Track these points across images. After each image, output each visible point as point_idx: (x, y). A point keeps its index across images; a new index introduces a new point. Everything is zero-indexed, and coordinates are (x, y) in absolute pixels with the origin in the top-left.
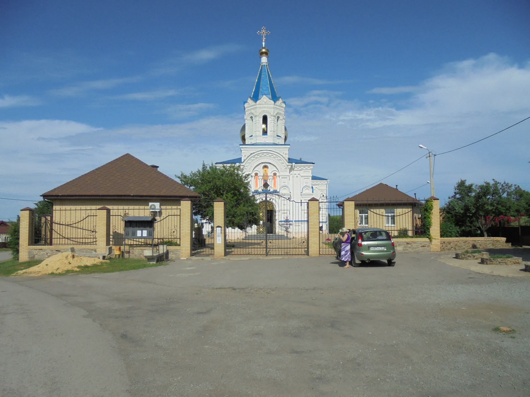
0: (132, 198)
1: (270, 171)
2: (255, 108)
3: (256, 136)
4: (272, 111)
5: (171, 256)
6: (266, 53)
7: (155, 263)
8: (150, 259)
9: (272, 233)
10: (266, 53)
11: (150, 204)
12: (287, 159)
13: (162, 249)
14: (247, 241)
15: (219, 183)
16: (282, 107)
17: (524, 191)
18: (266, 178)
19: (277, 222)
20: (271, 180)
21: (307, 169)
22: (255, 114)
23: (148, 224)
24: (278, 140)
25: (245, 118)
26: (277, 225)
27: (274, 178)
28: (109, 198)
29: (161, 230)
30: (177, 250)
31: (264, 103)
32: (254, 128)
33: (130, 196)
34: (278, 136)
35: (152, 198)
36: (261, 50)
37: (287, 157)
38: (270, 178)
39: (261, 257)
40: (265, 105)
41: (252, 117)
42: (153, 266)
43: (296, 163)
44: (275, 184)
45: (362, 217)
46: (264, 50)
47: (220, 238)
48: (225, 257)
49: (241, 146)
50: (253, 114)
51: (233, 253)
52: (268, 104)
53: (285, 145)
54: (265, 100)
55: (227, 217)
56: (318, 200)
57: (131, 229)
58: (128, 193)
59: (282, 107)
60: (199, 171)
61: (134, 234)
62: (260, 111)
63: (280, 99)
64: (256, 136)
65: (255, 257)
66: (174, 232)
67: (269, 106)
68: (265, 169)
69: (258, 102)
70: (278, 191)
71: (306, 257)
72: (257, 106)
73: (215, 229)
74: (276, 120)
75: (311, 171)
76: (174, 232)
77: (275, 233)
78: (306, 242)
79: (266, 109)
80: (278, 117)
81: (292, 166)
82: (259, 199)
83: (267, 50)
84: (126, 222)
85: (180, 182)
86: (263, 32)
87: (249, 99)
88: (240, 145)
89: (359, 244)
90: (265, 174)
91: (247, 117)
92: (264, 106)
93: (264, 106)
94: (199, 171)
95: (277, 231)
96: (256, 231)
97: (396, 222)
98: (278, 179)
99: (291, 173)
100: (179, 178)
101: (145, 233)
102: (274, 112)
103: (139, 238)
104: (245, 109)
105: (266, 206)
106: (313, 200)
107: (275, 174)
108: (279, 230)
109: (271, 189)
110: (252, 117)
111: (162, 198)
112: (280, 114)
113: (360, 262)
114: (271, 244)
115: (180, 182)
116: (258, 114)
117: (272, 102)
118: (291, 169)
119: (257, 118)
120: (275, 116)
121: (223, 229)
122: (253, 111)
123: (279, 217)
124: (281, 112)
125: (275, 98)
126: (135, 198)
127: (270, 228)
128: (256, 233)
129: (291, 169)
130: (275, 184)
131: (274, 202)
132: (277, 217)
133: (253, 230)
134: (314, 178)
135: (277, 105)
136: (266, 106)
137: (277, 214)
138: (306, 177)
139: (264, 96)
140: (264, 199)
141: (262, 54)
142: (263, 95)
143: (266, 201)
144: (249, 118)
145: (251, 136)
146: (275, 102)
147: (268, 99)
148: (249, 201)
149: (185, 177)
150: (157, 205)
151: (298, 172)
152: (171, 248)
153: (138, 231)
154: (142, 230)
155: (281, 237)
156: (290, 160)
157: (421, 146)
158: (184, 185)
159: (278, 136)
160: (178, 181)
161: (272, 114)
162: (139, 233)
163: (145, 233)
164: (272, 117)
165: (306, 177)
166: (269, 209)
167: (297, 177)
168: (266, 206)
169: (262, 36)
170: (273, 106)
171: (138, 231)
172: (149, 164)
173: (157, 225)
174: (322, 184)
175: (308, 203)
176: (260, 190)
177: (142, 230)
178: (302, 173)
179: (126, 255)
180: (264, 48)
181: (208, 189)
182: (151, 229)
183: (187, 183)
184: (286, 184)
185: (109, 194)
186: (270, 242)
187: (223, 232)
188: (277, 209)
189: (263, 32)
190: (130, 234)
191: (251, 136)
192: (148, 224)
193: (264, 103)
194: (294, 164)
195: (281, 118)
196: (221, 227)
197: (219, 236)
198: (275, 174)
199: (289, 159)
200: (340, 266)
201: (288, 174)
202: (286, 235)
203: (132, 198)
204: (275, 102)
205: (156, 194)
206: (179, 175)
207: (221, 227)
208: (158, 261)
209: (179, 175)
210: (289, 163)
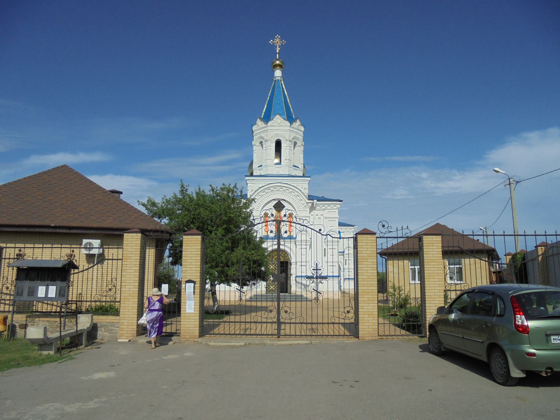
0: (54, 231)
3: (266, 166)
5: (101, 334)
6: (280, 66)
7: (52, 353)
8: (44, 344)
9: (287, 292)
10: (280, 66)
11: (85, 241)
12: (307, 195)
13: (84, 322)
14: (254, 304)
15: (205, 214)
16: (301, 131)
19: (293, 278)
21: (332, 209)
22: (266, 138)
23: (61, 274)
24: (295, 171)
25: (253, 143)
28: (11, 229)
29: (86, 285)
30: (113, 324)
31: (277, 125)
32: (262, 156)
33: (49, 227)
34: (294, 166)
35: (88, 232)
36: (274, 62)
37: (306, 192)
39: (268, 341)
40: (279, 127)
41: (261, 143)
42: (49, 360)
43: (318, 201)
45: (414, 271)
46: (278, 62)
47: (192, 303)
48: (200, 340)
49: (246, 178)
50: (263, 138)
51: (216, 331)
53: (303, 176)
54: (279, 122)
55: (206, 263)
56: (375, 234)
57: (27, 284)
58: (46, 222)
59: (301, 131)
60: (175, 197)
61: (33, 292)
63: (298, 121)
65: (256, 340)
66: (110, 290)
69: (270, 123)
71: (353, 340)
72: (269, 128)
73: (183, 286)
74: (293, 146)
75: (337, 211)
76: (110, 290)
77: (290, 293)
78: (352, 311)
79: (280, 132)
80: (295, 144)
81: (313, 204)
82: (269, 246)
83: (282, 62)
84: (19, 269)
85: (146, 212)
86: (277, 41)
87: (259, 120)
88: (246, 176)
89: (517, 327)
91: (256, 142)
92: (278, 128)
93: (278, 128)
94: (175, 197)
95: (293, 289)
96: (265, 289)
97: (464, 277)
99: (312, 213)
100: (143, 205)
101: (53, 291)
102: (290, 136)
103: (42, 300)
104: (253, 132)
105: (279, 256)
106: (366, 232)
108: (294, 288)
110: (261, 143)
111: (108, 232)
112: (298, 139)
113: (523, 375)
114: (287, 315)
115: (146, 212)
116: (269, 138)
117: (288, 123)
118: (312, 208)
119: (268, 143)
120: (291, 141)
121: (198, 285)
122: (262, 135)
124: (298, 136)
125: (290, 119)
126: (58, 231)
127: (284, 287)
128: (264, 293)
129: (312, 208)
131: (287, 250)
133: (261, 287)
134: (340, 224)
135: (293, 128)
136: (280, 128)
137: (293, 266)
138: (331, 219)
139: (278, 116)
140: (276, 247)
141: (275, 66)
142: (275, 115)
143: (279, 250)
144: (258, 144)
145: (261, 166)
146: (291, 123)
147: (282, 120)
148: (250, 241)
149: (154, 204)
150: (96, 243)
152: (100, 319)
153: (40, 288)
154: (47, 286)
155: (300, 298)
156: (310, 198)
157: (496, 169)
158: (153, 217)
159: (294, 166)
160: (143, 209)
161: (287, 138)
162: (41, 291)
163: (53, 291)
164: (288, 142)
165: (331, 219)
166: (282, 260)
167: (319, 218)
168: (279, 256)
169: (276, 46)
170: (289, 128)
171: (40, 288)
172: (108, 188)
173: (74, 278)
175: (355, 239)
177: (47, 286)
178: (326, 214)
179: (20, 332)
180: (278, 60)
181: (185, 221)
182: (64, 284)
183: (155, 214)
185: (13, 223)
186: (286, 312)
187: (198, 291)
188: (293, 260)
189: (277, 41)
190: (26, 292)
191: (261, 166)
192: (61, 274)
193: (277, 125)
194: (315, 201)
195: (299, 143)
196: (194, 282)
197: (190, 299)
199: (309, 196)
202: (305, 296)
203: (54, 231)
204: (291, 123)
205: (95, 225)
206: (145, 201)
207: (194, 282)
208: (59, 350)
209: (145, 201)
210: (309, 199)
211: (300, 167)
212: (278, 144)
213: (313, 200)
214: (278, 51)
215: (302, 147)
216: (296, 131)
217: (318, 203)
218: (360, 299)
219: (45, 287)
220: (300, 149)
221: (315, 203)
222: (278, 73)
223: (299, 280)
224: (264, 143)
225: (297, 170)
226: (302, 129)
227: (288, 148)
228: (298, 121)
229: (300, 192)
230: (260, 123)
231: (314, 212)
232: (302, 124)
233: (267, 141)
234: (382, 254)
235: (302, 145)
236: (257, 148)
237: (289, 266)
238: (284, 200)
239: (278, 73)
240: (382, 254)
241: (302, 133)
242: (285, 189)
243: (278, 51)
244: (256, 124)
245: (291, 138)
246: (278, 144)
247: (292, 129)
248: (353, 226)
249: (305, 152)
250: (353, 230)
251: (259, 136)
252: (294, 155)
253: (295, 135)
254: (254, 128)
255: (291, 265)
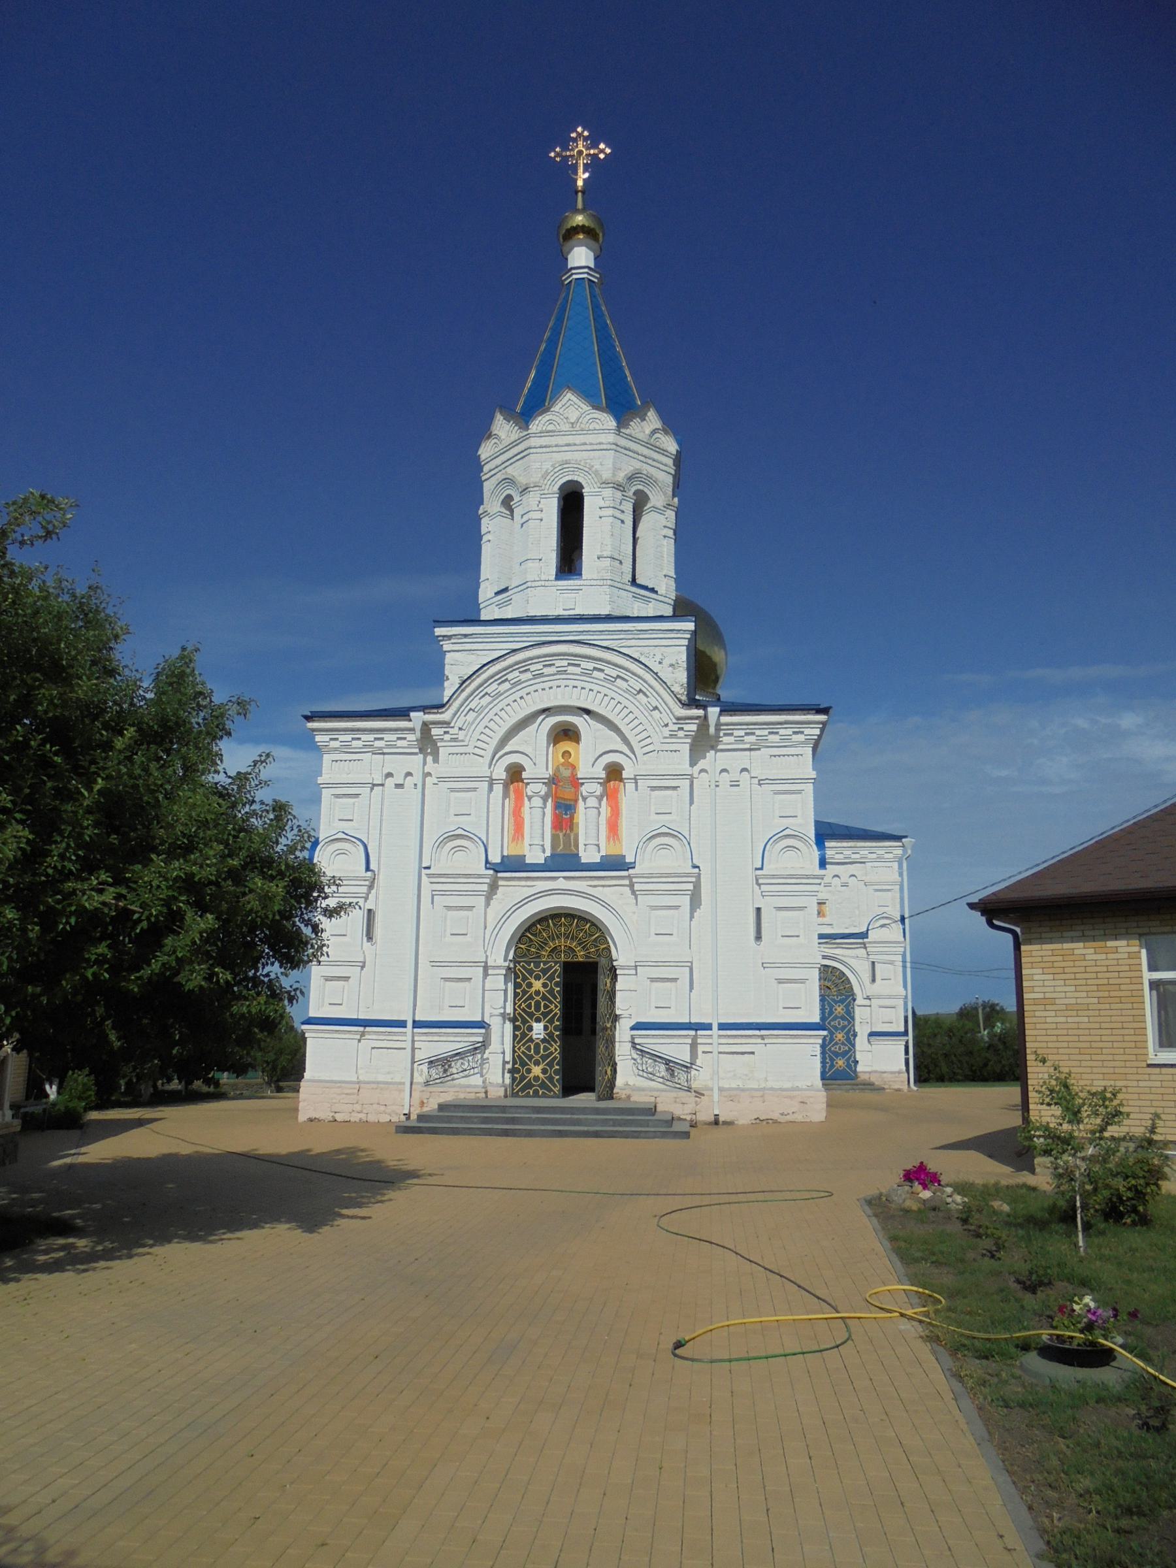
1: (590, 754)
2: (523, 455)
3: (524, 586)
4: (609, 463)
16: (664, 452)
17: (985, 1186)
18: (567, 792)
19: (623, 1032)
20: (592, 802)
21: (786, 743)
22: (522, 480)
26: (623, 1050)
27: (611, 796)
31: (567, 427)
36: (565, 220)
38: (584, 790)
40: (573, 441)
41: (507, 502)
44: (613, 828)
46: (579, 219)
52: (588, 432)
54: (573, 415)
59: (664, 452)
62: (547, 466)
63: (652, 414)
64: (524, 586)
67: (590, 439)
68: (566, 746)
69: (539, 424)
70: (629, 859)
72: (533, 442)
74: (628, 507)
90: (566, 773)
91: (491, 504)
98: (628, 795)
102: (616, 469)
107: (614, 772)
108: (630, 1076)
109: (591, 845)
112: (650, 480)
116: (535, 477)
118: (703, 742)
119: (532, 499)
120: (618, 487)
123: (632, 1000)
125: (621, 408)
129: (703, 742)
130: (613, 828)
132: (620, 1006)
135: (630, 438)
136: (578, 439)
151: (743, 759)
161: (607, 475)
164: (608, 492)
167: (735, 784)
170: (612, 438)
174: (880, 859)
176: (536, 857)
178: (761, 763)
184: (675, 821)
188: (622, 956)
193: (567, 427)
194: (713, 711)
198: (614, 772)
200: (1039, 1354)
201: (685, 767)
211: (662, 591)
212: (571, 504)
213: (704, 707)
214: (580, 183)
215: (671, 514)
216: (646, 452)
217: (725, 719)
218: (1026, 1020)
219: (816, 1018)
220: (659, 526)
221: (712, 721)
222: (581, 257)
223: (650, 1040)
224: (516, 498)
225: (647, 600)
226: (672, 446)
227: (610, 512)
228: (652, 414)
229: (648, 677)
230: (503, 428)
231: (710, 760)
232: (670, 425)
233: (525, 490)
234: (994, 910)
235: (668, 506)
236: (493, 526)
237: (603, 981)
238: (587, 712)
239: (581, 257)
240: (994, 910)
241: (670, 462)
242: (590, 666)
243: (580, 183)
244: (490, 436)
245: (621, 477)
246: (571, 504)
247: (623, 442)
248: (898, 838)
249: (680, 534)
250: (899, 852)
251: (500, 476)
252: (634, 548)
253: (638, 465)
254: (486, 451)
255: (614, 977)
